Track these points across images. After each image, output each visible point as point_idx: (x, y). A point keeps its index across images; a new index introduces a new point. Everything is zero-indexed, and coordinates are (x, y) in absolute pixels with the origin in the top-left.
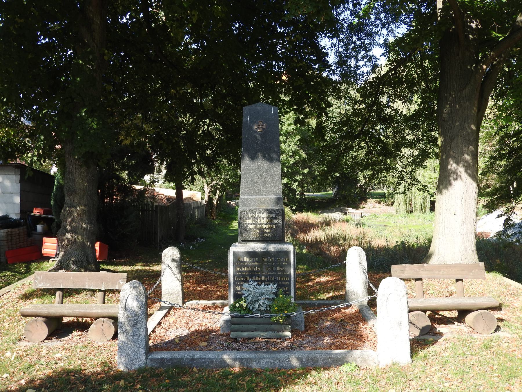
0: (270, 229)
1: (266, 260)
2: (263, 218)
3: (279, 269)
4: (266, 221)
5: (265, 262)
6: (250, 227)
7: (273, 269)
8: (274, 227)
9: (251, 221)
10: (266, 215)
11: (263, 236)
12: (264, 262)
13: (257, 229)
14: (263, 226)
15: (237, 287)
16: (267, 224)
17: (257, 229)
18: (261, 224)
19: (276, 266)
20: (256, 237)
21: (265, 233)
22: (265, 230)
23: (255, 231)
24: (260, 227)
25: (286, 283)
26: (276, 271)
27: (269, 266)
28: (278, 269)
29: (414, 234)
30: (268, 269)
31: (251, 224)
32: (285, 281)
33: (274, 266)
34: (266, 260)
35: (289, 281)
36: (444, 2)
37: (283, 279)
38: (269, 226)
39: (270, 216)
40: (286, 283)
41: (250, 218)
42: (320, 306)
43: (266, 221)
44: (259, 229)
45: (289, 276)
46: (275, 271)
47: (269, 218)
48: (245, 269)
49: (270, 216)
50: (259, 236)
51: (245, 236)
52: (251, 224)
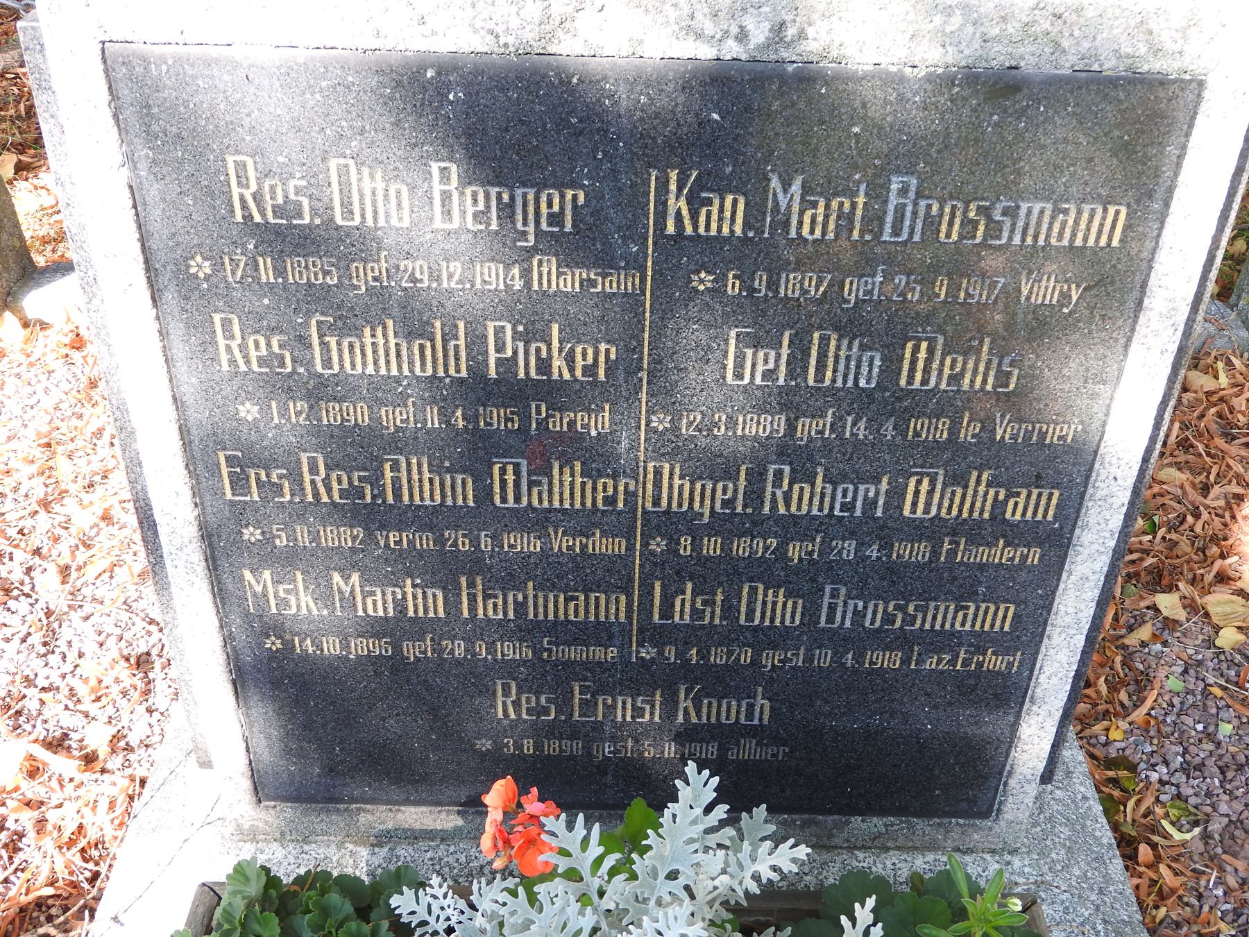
1: (727, 216)
3: (925, 367)
5: (712, 251)
7: (850, 365)
12: (682, 251)
15: (258, 582)
19: (885, 330)
25: (1001, 554)
26: (889, 402)
27: (765, 319)
28: (912, 378)
29: (1245, 539)
30: (760, 366)
32: (998, 527)
33: (850, 324)
34: (727, 216)
35: (1056, 541)
37: (978, 498)
40: (1001, 554)
45: (1066, 471)
46: (860, 402)
48: (374, 355)
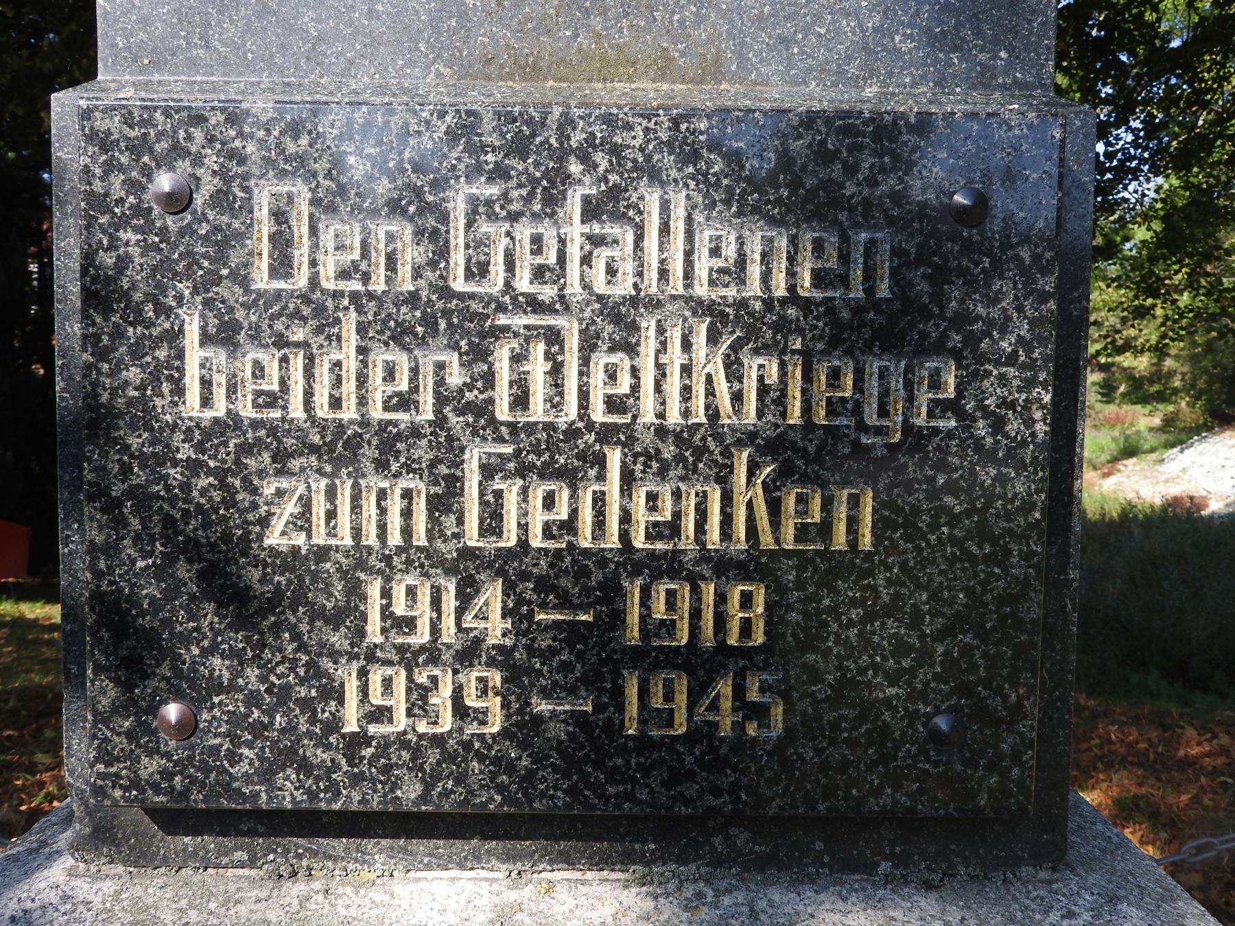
0: (753, 565)
2: (618, 322)
4: (681, 378)
6: (298, 515)
8: (855, 518)
9: (348, 379)
10: (684, 245)
11: (595, 737)
13: (468, 571)
14: (615, 510)
16: (695, 451)
17: (468, 571)
18: (559, 456)
20: (453, 752)
21: (652, 657)
22: (647, 605)
23: (418, 603)
24: (529, 514)
31: (339, 448)
36: (1180, 528)
38: (732, 509)
39: (770, 263)
41: (318, 311)
42: (791, 259)
43: (681, 378)
44: (510, 565)
47: (743, 326)
49: (770, 263)
50: (523, 728)
51: (220, 706)
52: (339, 448)
